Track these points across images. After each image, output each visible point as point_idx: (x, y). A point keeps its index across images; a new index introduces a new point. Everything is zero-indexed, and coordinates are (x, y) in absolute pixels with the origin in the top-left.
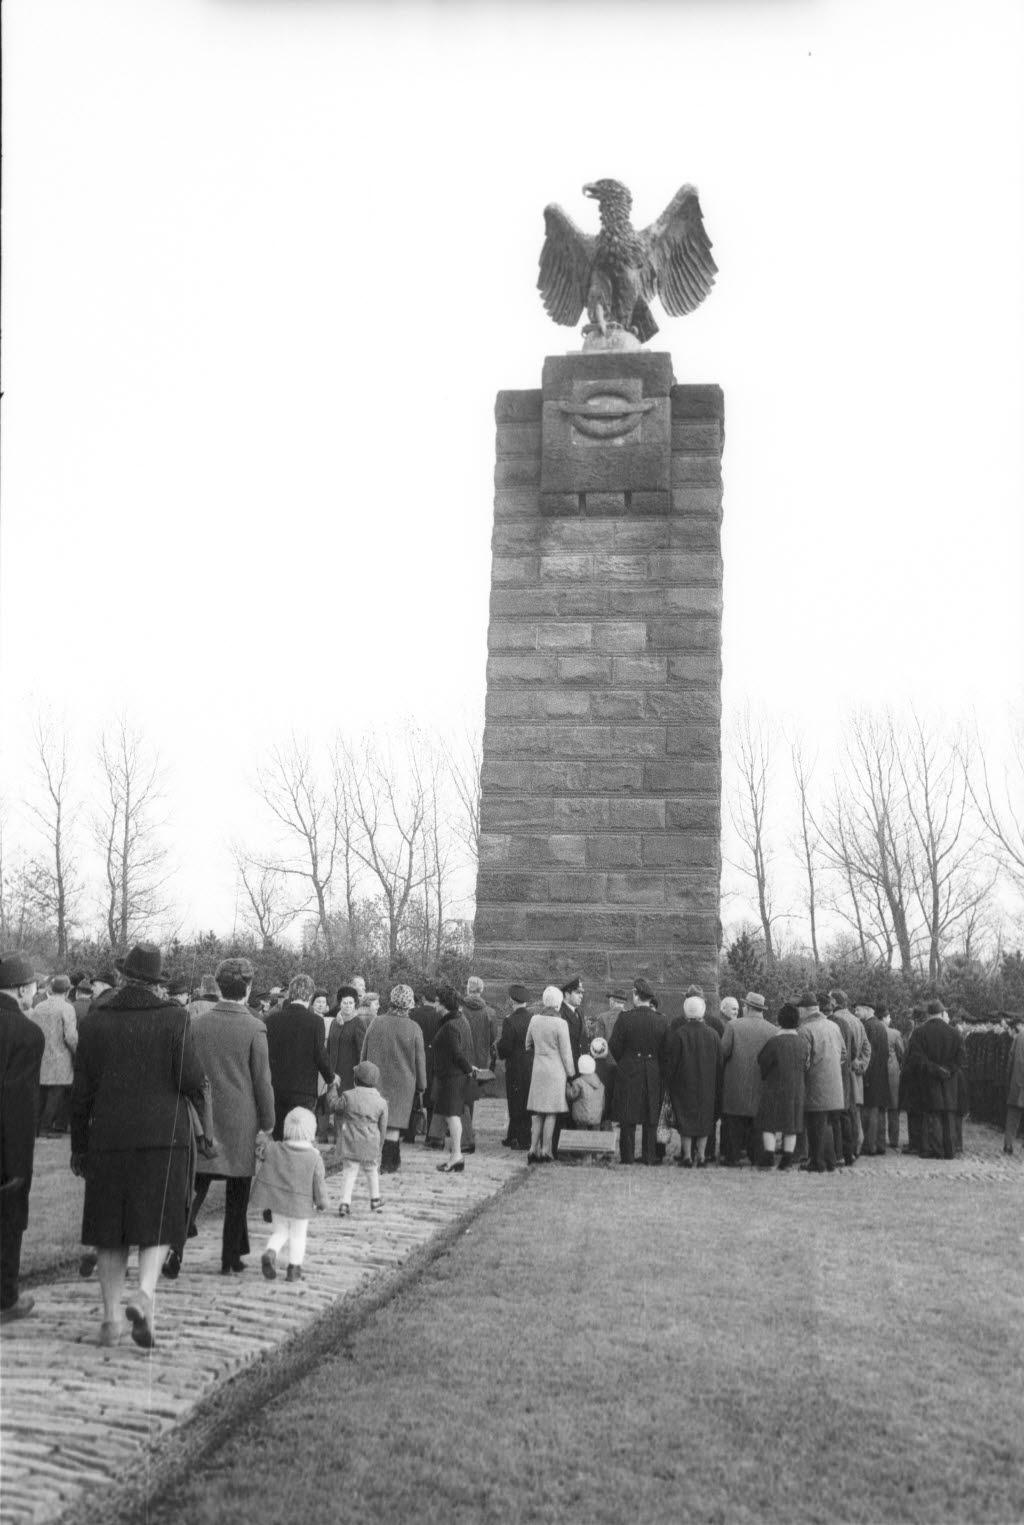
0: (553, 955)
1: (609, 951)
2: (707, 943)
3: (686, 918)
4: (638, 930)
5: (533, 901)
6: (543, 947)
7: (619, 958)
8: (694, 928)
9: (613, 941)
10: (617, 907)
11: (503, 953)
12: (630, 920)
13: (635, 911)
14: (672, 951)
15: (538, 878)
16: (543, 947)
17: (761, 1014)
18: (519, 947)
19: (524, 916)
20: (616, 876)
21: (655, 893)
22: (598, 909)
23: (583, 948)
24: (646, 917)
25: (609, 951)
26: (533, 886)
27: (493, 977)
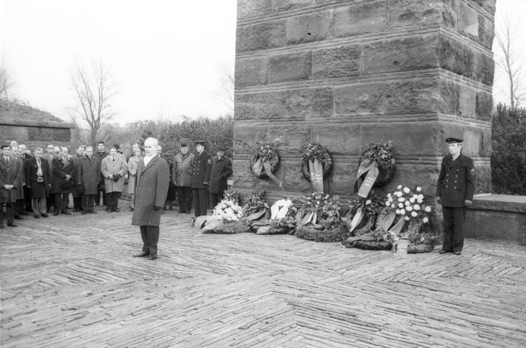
0: (289, 94)
1: (335, 86)
2: (428, 67)
3: (405, 42)
4: (361, 62)
5: (274, 46)
6: (282, 88)
7: (346, 91)
8: (413, 51)
9: (334, 75)
10: (344, 40)
11: (252, 96)
12: (354, 53)
13: (359, 41)
14: (392, 79)
15: (277, 24)
16: (282, 88)
17: (81, 139)
18: (263, 89)
19: (267, 62)
20: (340, 9)
21: (376, 21)
22: (324, 45)
23: (312, 85)
24: (367, 47)
25: (335, 86)
26: (273, 32)
27: (246, 119)
